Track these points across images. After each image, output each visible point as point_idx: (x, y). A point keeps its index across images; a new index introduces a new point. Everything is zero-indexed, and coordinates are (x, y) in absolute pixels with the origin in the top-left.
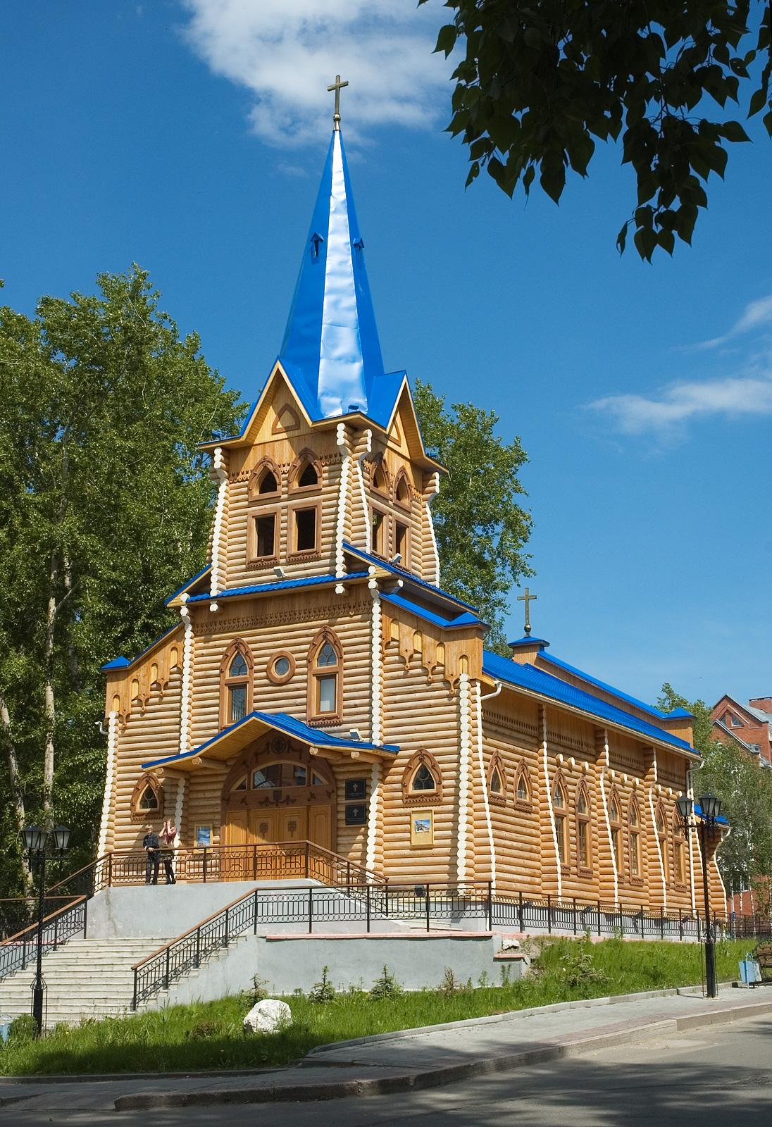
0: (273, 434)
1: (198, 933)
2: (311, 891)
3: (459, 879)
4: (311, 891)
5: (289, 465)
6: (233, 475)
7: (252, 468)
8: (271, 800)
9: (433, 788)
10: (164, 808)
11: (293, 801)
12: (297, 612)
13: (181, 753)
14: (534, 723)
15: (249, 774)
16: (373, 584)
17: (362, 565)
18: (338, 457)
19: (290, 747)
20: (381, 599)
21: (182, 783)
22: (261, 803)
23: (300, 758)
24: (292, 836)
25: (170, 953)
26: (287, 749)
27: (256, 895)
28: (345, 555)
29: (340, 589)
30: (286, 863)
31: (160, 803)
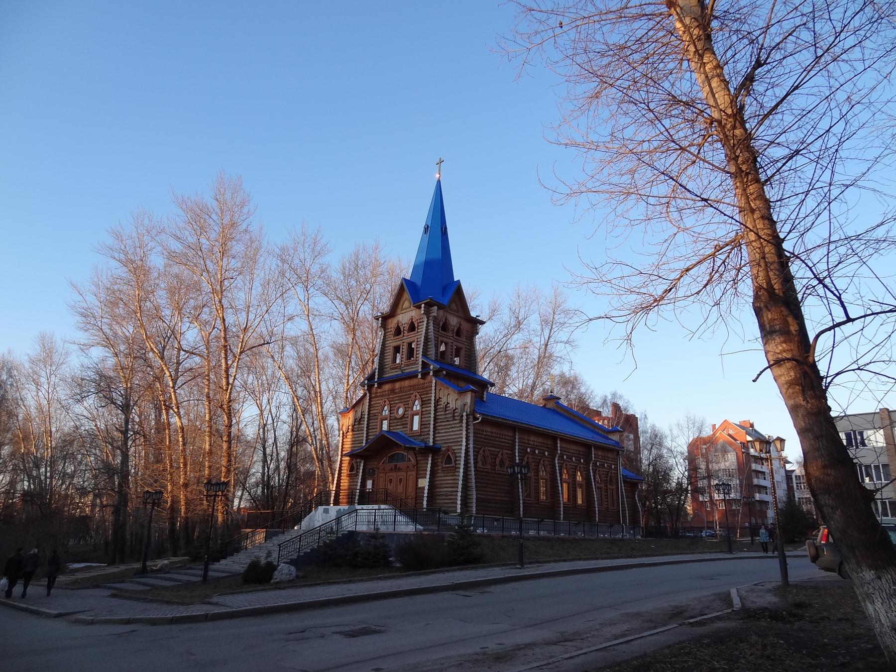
1: (300, 539)
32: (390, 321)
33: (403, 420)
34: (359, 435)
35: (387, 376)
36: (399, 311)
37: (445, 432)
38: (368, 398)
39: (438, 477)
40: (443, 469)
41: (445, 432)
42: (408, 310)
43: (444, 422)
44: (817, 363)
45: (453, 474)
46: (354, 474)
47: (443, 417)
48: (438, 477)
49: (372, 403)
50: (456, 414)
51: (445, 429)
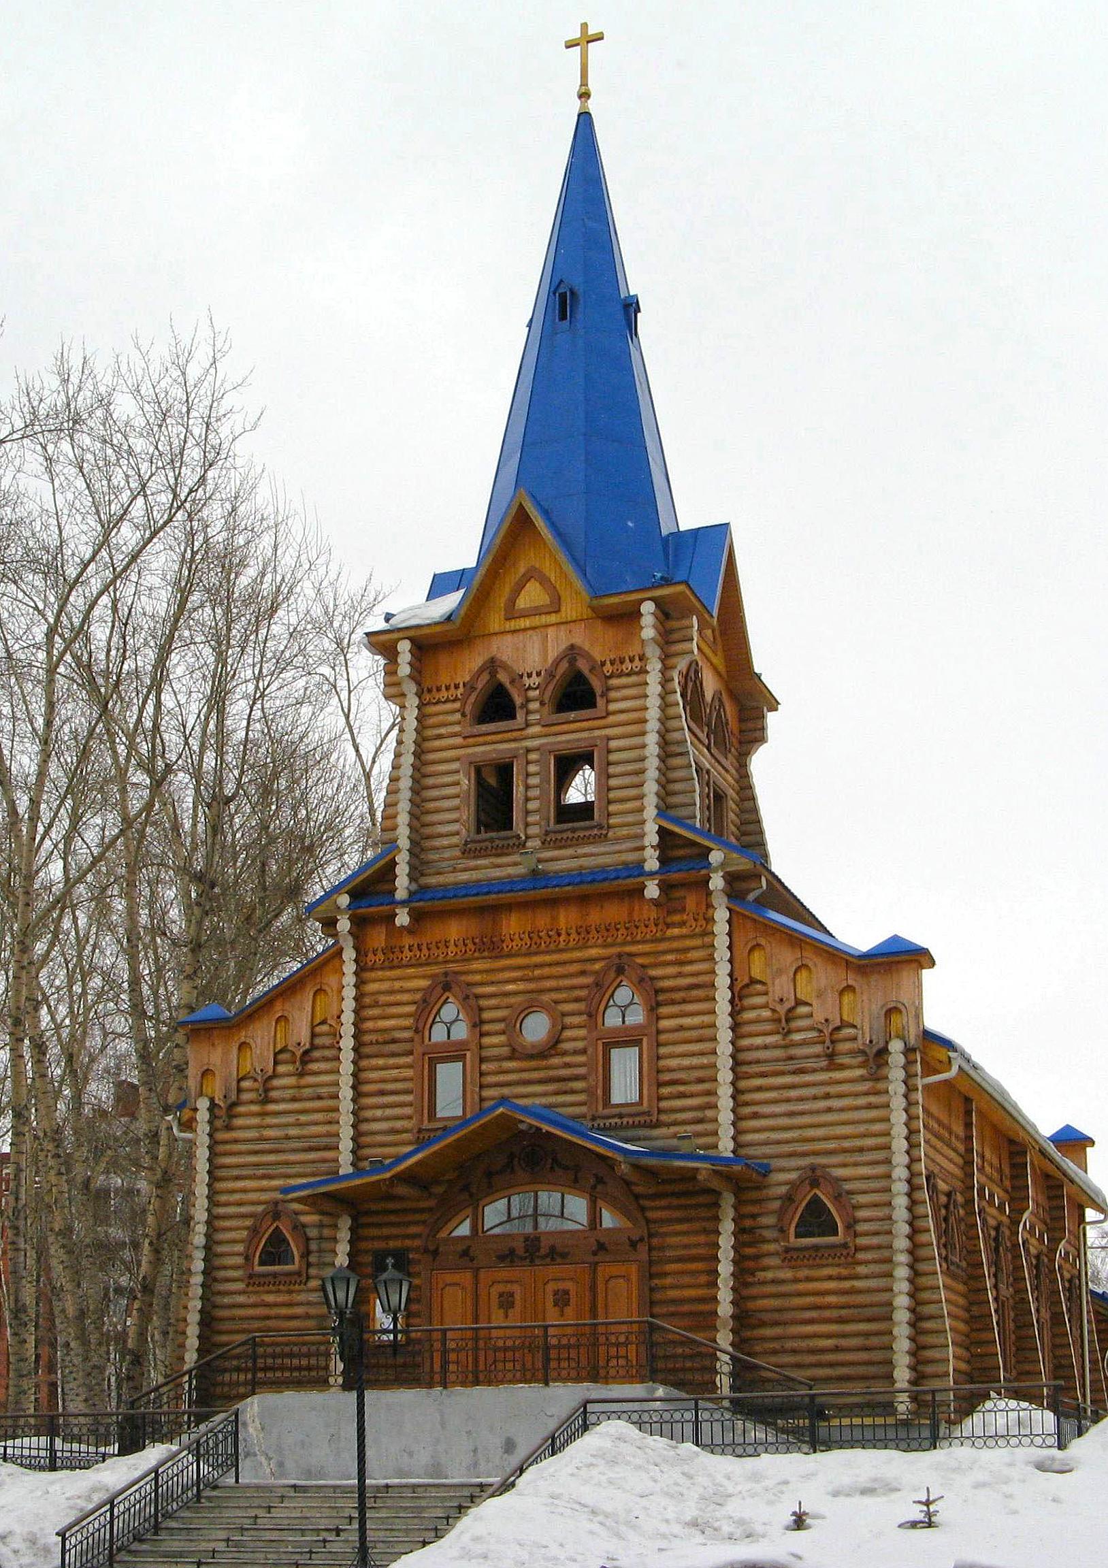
0: (508, 619)
1: (156, 1479)
2: (696, 1404)
3: (898, 1385)
4: (696, 1404)
5: (538, 674)
6: (430, 691)
7: (467, 679)
8: (521, 1252)
9: (836, 1234)
10: (309, 1265)
11: (564, 1255)
12: (563, 932)
13: (341, 1172)
14: (959, 1129)
15: (476, 1208)
16: (717, 882)
17: (695, 851)
18: (637, 662)
19: (555, 1160)
20: (730, 910)
21: (345, 1223)
22: (502, 1258)
23: (576, 1180)
24: (507, 1317)
25: (116, 1510)
26: (548, 1166)
27: (585, 1412)
28: (662, 832)
29: (652, 890)
30: (495, 1361)
31: (302, 1257)
32: (444, 659)
33: (556, 1061)
34: (303, 1118)
35: (441, 879)
36: (495, 621)
37: (791, 1114)
38: (350, 968)
39: (763, 1283)
40: (790, 1256)
41: (791, 1114)
42: (545, 619)
43: (782, 1073)
44: (681, 529)
45: (844, 1272)
46: (299, 1274)
47: (778, 1053)
48: (763, 1283)
49: (372, 987)
50: (843, 1047)
51: (788, 1100)
